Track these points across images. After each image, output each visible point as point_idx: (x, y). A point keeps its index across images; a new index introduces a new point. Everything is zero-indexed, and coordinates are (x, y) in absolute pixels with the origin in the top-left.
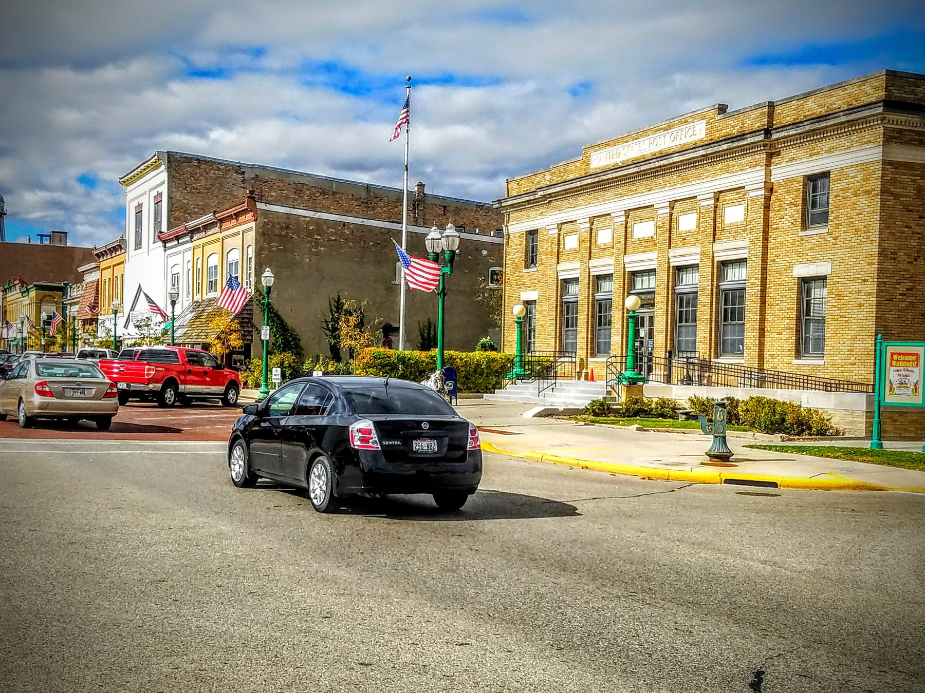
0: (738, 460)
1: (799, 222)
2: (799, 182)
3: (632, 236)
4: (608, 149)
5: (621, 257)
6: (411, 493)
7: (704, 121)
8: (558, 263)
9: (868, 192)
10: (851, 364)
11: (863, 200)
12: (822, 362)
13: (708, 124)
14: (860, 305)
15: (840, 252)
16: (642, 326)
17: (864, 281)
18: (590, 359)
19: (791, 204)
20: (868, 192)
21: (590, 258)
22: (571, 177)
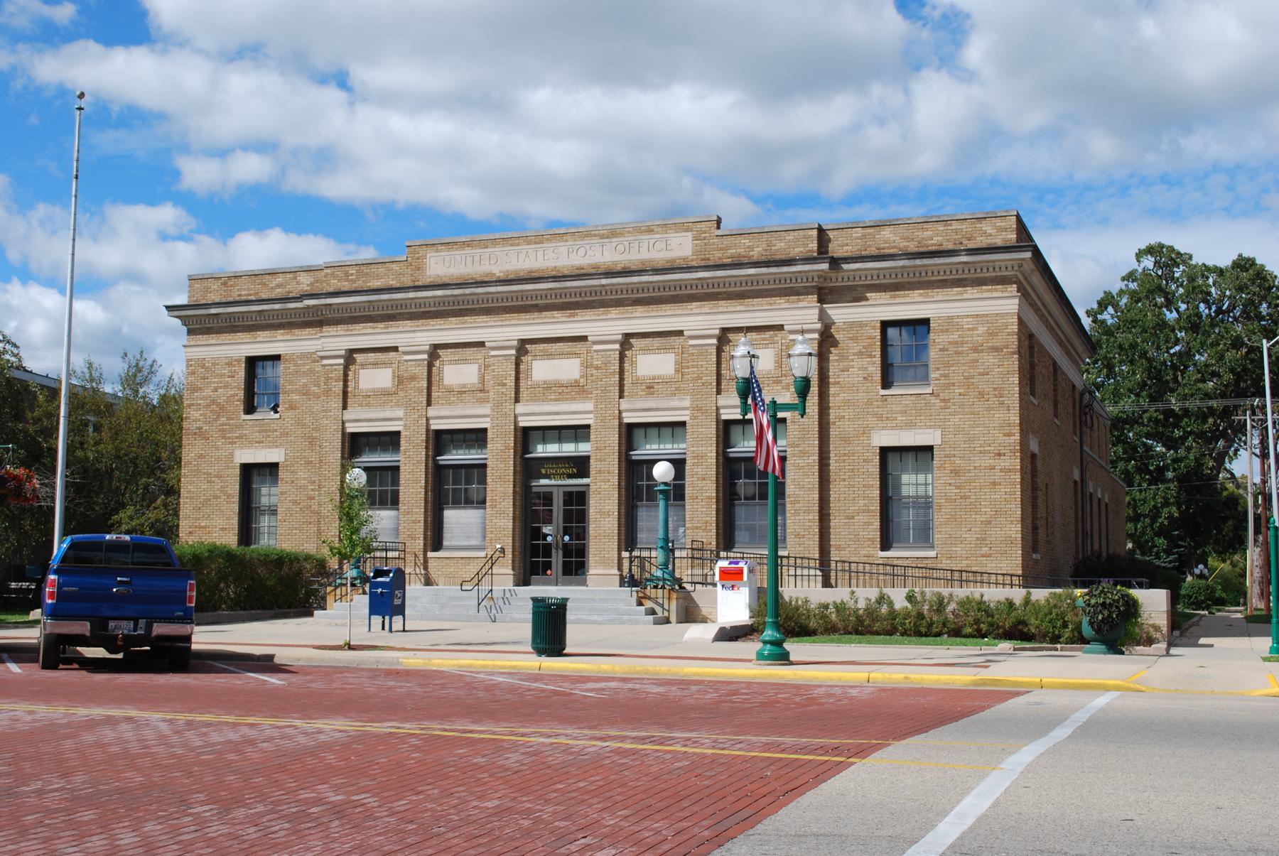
0: (752, 372)
1: (877, 376)
2: (874, 328)
3: (528, 377)
4: (468, 251)
5: (509, 406)
6: (104, 659)
7: (690, 234)
8: (345, 408)
9: (996, 349)
10: (983, 556)
11: (990, 359)
12: (932, 554)
13: (695, 239)
14: (994, 484)
15: (956, 419)
16: (421, 685)
17: (999, 455)
18: (430, 554)
19: (860, 354)
20: (996, 349)
21: (429, 403)
22: (377, 284)
